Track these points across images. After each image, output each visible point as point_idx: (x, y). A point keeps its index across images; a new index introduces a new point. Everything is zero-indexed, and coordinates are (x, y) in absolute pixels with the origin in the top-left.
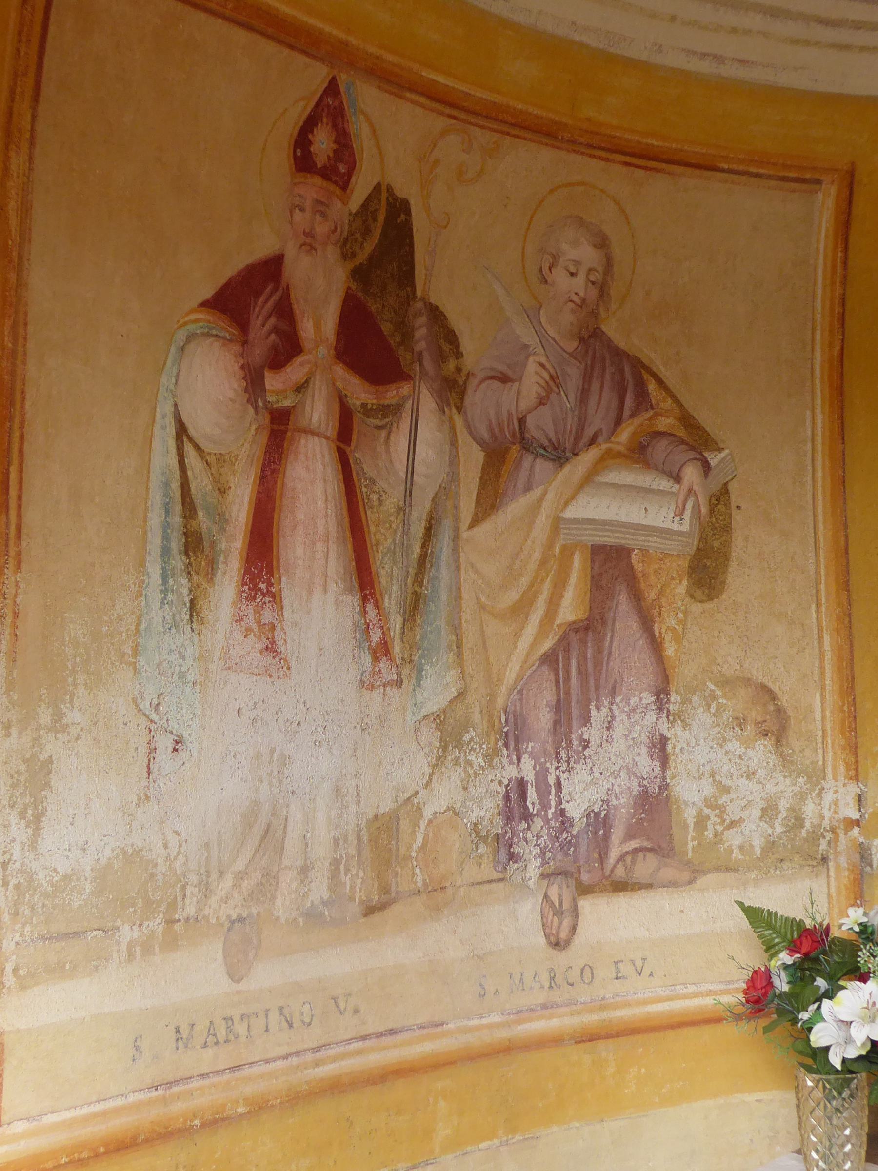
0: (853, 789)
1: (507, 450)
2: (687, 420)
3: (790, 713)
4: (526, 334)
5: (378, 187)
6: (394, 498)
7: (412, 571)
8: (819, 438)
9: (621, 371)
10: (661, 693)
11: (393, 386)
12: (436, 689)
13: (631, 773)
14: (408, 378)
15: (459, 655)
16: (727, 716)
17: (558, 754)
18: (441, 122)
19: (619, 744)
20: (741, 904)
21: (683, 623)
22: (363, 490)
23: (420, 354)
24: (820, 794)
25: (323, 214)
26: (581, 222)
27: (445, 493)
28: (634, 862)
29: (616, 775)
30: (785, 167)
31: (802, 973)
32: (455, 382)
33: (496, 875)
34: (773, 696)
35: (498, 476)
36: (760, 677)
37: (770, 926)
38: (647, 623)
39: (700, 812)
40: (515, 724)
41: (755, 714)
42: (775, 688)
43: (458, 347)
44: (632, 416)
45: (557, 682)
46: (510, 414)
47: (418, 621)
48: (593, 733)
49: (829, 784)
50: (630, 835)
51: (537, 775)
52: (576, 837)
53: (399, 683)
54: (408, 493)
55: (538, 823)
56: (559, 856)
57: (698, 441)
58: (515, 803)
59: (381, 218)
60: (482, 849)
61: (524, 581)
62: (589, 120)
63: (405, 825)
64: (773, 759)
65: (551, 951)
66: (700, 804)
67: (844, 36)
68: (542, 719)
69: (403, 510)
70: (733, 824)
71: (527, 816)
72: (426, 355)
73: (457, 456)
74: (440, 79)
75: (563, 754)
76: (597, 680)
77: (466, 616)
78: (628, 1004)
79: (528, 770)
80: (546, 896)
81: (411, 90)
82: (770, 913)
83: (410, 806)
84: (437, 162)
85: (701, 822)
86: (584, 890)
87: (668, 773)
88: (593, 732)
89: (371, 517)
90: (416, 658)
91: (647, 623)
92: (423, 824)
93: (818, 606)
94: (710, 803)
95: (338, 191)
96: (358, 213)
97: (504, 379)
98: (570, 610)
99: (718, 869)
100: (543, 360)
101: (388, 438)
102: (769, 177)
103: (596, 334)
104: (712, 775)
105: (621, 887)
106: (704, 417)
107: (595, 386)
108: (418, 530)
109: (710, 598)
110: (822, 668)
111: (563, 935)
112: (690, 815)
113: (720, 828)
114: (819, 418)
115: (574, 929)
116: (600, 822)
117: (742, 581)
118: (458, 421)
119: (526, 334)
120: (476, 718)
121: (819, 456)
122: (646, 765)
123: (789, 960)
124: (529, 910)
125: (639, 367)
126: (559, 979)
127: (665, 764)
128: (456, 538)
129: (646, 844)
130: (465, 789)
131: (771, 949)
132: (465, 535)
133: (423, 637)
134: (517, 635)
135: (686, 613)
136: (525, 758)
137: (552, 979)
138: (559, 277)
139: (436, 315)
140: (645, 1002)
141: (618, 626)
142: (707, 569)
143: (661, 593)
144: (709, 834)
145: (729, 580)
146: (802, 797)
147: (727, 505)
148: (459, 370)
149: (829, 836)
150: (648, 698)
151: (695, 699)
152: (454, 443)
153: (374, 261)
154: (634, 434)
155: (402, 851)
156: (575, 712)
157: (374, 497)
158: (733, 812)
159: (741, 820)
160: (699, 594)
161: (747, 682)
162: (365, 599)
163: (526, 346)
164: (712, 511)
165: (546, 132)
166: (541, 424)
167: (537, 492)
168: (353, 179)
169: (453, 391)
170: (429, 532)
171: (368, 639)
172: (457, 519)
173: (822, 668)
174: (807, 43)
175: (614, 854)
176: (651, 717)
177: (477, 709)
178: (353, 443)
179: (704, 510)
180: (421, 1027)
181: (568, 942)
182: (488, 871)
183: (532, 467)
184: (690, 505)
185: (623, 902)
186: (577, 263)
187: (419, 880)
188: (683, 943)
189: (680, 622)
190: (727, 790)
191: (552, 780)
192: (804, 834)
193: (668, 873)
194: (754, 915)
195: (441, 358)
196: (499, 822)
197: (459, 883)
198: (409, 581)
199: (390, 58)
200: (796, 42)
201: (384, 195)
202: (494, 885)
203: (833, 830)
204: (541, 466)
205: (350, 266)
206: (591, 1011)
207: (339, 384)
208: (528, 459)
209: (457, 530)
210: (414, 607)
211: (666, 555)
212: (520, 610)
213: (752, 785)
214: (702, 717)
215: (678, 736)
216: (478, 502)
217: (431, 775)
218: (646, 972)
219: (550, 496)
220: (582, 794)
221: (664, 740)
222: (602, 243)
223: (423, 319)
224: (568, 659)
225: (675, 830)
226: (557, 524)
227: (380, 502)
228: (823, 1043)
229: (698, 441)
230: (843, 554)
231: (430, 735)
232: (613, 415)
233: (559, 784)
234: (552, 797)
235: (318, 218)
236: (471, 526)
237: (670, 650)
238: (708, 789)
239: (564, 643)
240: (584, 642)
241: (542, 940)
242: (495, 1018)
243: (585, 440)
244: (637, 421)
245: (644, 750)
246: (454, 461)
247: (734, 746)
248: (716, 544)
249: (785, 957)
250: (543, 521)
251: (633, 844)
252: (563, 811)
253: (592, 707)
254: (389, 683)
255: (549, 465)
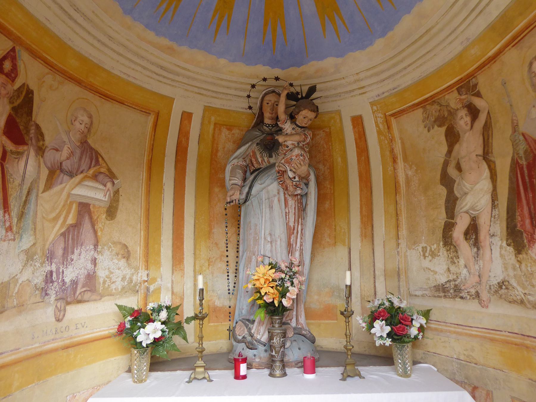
0: (146, 272)
1: (56, 171)
2: (109, 170)
3: (131, 252)
4: (66, 139)
5: (24, 84)
6: (18, 181)
7: (22, 205)
8: (144, 180)
9: (92, 154)
10: (96, 246)
11: (21, 146)
12: (26, 242)
13: (85, 268)
14: (27, 144)
15: (35, 232)
16: (114, 252)
17: (63, 263)
18: (47, 70)
19: (82, 260)
20: (116, 305)
21: (104, 226)
22: (8, 177)
23: (31, 138)
24: (137, 274)
25: (4, 88)
26: (85, 110)
27: (35, 182)
28: (84, 294)
29: (80, 269)
30: (142, 108)
31: (134, 322)
32: (42, 148)
33: (41, 300)
34: (127, 248)
35: (52, 178)
36: (124, 242)
37: (125, 310)
38: (93, 226)
39: (104, 279)
40: (51, 253)
41: (122, 252)
42: (128, 245)
43: (44, 138)
44: (94, 167)
45: (65, 241)
46: (58, 161)
47: (22, 220)
48: (75, 257)
49: (140, 271)
50: (83, 287)
51: (56, 269)
52: (67, 288)
53: (14, 240)
54: (23, 180)
55: (56, 284)
56: (61, 293)
57: (112, 176)
58: (49, 278)
59: (24, 93)
60: (37, 292)
61: (58, 211)
62: (91, 82)
63: (12, 285)
64: (126, 264)
65: (56, 323)
66: (105, 277)
67: (161, 79)
68: (60, 252)
69: (21, 185)
70: (113, 282)
71: (52, 282)
72: (33, 138)
73: (40, 171)
74: (49, 58)
75: (65, 263)
76: (77, 241)
77: (38, 220)
78: (79, 336)
79: (54, 268)
80: (56, 306)
81: (39, 58)
82: (125, 306)
83: (14, 279)
84: (44, 82)
85: (104, 282)
86: (68, 303)
87: (96, 268)
88: (75, 256)
89: (10, 186)
90: (20, 232)
91: (93, 226)
92: (18, 285)
93: (141, 223)
94: (107, 277)
95: (11, 82)
96: (16, 90)
97: (57, 150)
98: (71, 220)
99: (108, 295)
100: (69, 146)
101: (18, 162)
102: (138, 110)
103: (86, 142)
104: (109, 269)
105: (79, 302)
106: (114, 170)
107: (84, 157)
108: (25, 192)
109: (112, 220)
110: (140, 240)
111: (61, 317)
112: (101, 280)
113: (109, 284)
114: (144, 174)
115: (64, 315)
116: (75, 283)
117: (121, 215)
118: (42, 160)
119: (66, 139)
120: (39, 251)
121: (144, 184)
122: (90, 266)
123: (131, 319)
124: (50, 311)
125: (97, 154)
126: (58, 331)
127: (95, 266)
128: (37, 196)
129: (88, 289)
130: (33, 273)
131: (125, 316)
132: (40, 195)
133: (23, 226)
134: (54, 227)
135: (105, 223)
136: (53, 264)
137: (56, 331)
138: (77, 124)
139: (38, 127)
140: (84, 335)
141: (85, 226)
142: (111, 212)
143: (98, 217)
144: (106, 285)
145: (117, 215)
146: (133, 274)
147: (118, 194)
148: (43, 145)
149: (139, 285)
150: (92, 247)
151: (105, 248)
152: (39, 167)
153: (20, 106)
154: (94, 172)
155: (10, 294)
156: (70, 250)
157: (11, 180)
158: (114, 279)
159: (116, 281)
160: (108, 218)
161: (120, 243)
162: (5, 212)
163: (65, 142)
164: (114, 196)
165: (78, 82)
166: (67, 165)
167: (64, 185)
168: (16, 79)
169: (41, 151)
170: (29, 193)
171: (5, 225)
172: (38, 190)
173: (140, 240)
174: (151, 78)
175: (78, 292)
176: (92, 252)
177: (39, 249)
178: (6, 162)
179: (112, 195)
180: (11, 351)
181: (62, 319)
182: (38, 299)
183: (63, 178)
184: (108, 193)
185: (80, 306)
186: (83, 121)
187: (15, 303)
188: (99, 316)
189: (103, 226)
190: (112, 273)
191: (61, 271)
192: (133, 284)
193: (94, 297)
194: (120, 307)
195: (38, 140)
196: (43, 284)
197: (29, 303)
198: (21, 208)
199: (34, 46)
200: (149, 77)
201: (26, 87)
202: (40, 304)
203: (140, 283)
204: (66, 178)
205: (12, 106)
206: (67, 340)
207: (3, 142)
208: (62, 175)
209: (38, 193)
210: (21, 216)
211: (100, 207)
212: (56, 219)
213: (120, 272)
214: (107, 253)
215: (100, 258)
216: (45, 185)
217: (22, 269)
218: (85, 326)
219: (68, 187)
220: (70, 274)
221: (95, 259)
222: (90, 117)
223: (33, 128)
224: (69, 235)
225: (97, 285)
226: (69, 195)
227: (13, 182)
228: (141, 340)
229: (112, 176)
230: (148, 211)
231: (23, 257)
232: (88, 166)
233: (63, 272)
234: (61, 276)
235: (3, 88)
236: (43, 192)
237: (99, 234)
238: (107, 273)
239: (68, 230)
240: (74, 230)
241: (54, 319)
242: (37, 345)
243: (80, 171)
244: (95, 168)
245: (89, 262)
246: (39, 172)
247: (116, 261)
248: (115, 205)
249: (129, 318)
250: (65, 193)
251: (84, 289)
252: (64, 280)
253: (75, 249)
254: (11, 240)
255: (68, 177)
